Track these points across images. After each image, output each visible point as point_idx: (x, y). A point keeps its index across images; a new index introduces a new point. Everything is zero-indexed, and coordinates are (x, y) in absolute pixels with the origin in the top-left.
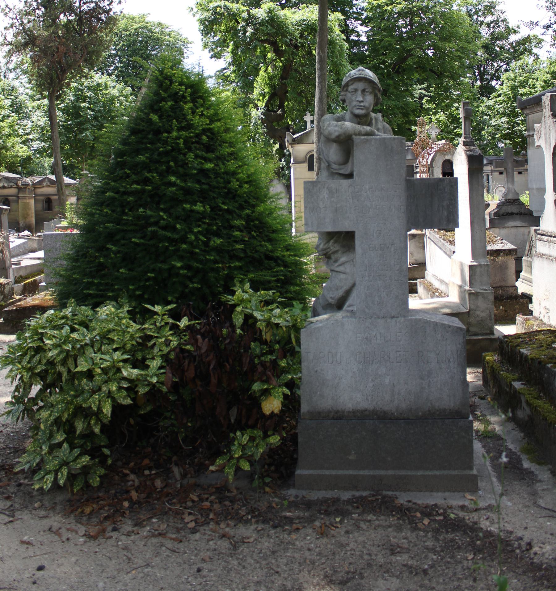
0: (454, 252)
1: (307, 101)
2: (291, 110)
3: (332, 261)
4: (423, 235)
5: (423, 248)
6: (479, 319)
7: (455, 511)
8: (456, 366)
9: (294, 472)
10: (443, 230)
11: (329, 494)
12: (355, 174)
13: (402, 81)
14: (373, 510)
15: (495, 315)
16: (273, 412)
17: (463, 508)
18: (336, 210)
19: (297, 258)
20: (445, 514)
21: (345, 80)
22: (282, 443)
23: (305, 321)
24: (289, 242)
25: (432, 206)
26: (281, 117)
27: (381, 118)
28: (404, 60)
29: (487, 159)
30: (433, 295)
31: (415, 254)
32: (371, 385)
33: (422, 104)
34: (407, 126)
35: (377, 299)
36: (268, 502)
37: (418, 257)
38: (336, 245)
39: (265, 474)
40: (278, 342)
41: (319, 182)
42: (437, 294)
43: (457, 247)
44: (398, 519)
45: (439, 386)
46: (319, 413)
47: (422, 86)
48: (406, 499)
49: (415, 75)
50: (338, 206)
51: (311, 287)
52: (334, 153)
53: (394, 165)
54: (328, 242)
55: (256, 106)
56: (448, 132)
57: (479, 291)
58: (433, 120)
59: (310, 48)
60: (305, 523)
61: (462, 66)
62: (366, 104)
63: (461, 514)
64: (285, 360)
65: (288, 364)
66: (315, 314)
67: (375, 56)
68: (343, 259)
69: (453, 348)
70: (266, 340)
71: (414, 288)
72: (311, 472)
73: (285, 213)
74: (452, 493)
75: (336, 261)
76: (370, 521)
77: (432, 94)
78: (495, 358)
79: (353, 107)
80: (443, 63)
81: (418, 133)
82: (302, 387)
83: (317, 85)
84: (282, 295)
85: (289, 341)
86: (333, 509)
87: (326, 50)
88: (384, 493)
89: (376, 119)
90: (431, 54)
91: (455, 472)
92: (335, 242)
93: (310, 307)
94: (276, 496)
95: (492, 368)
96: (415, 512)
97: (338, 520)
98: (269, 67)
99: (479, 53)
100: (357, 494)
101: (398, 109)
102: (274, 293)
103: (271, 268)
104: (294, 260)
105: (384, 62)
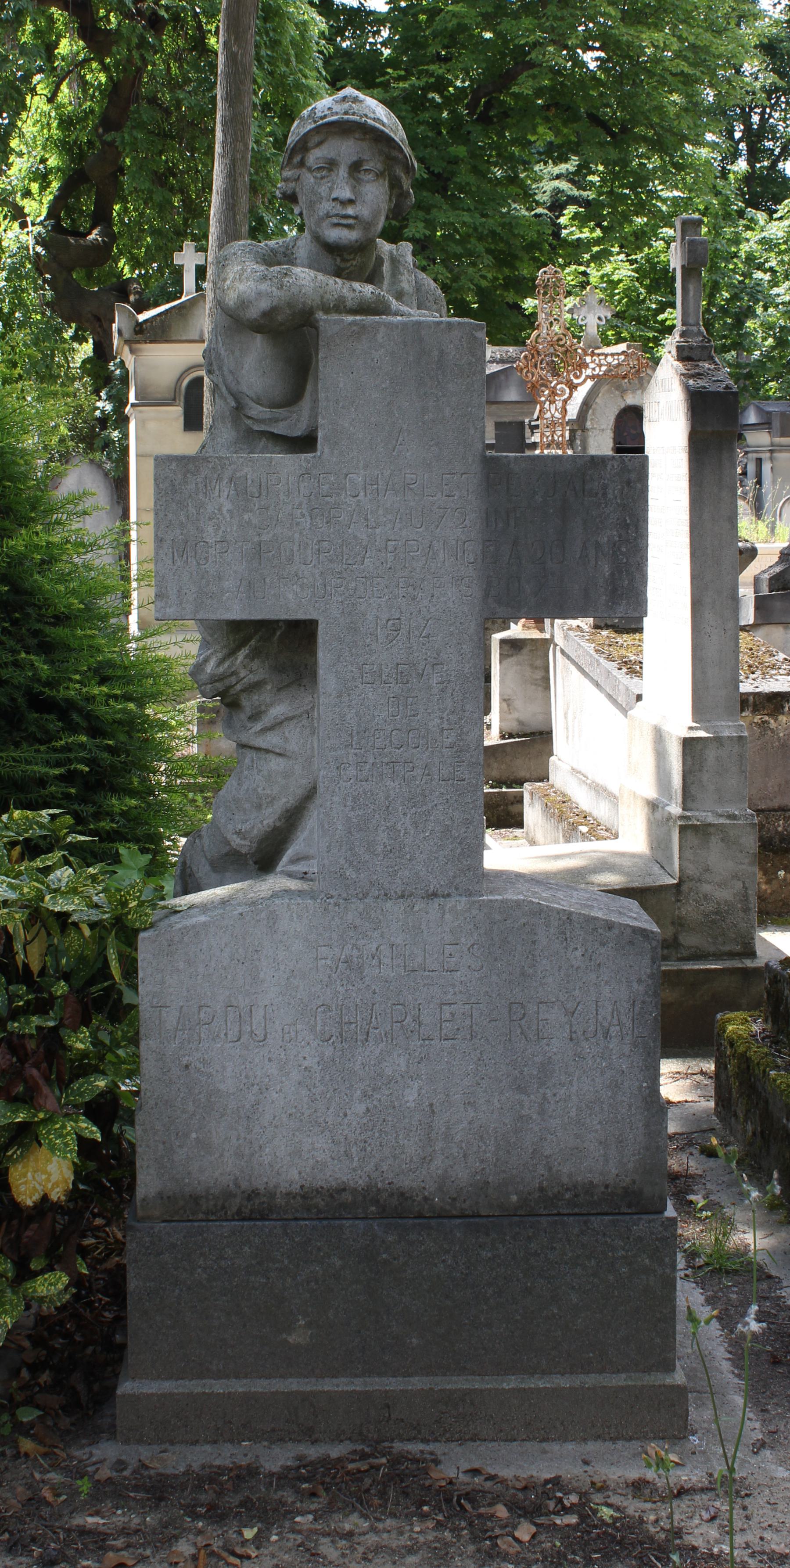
0: (639, 698)
1: (187, 203)
2: (135, 232)
3: (243, 716)
4: (546, 644)
5: (545, 683)
6: (710, 907)
7: (614, 1499)
8: (627, 1049)
9: (115, 1388)
10: (607, 627)
11: (226, 1455)
12: (320, 434)
13: (500, 149)
14: (360, 1502)
15: (761, 898)
16: (45, 1198)
17: (638, 1487)
18: (258, 551)
19: (132, 706)
20: (584, 1510)
21: (298, 130)
22: (76, 1297)
23: (154, 906)
24: (110, 653)
25: (562, 543)
26: (102, 254)
27: (410, 258)
28: (508, 78)
29: (759, 410)
30: (571, 833)
31: (518, 703)
32: (361, 1108)
33: (559, 227)
34: (510, 297)
35: (382, 837)
36: (29, 1487)
37: (527, 713)
38: (255, 664)
39: (18, 1398)
40: (66, 977)
41: (206, 460)
42: (584, 829)
43: (649, 683)
44: (439, 1525)
45: (573, 1113)
46: (195, 1199)
47: (563, 168)
48: (466, 1466)
49: (541, 129)
50: (264, 538)
51: (177, 800)
52: (256, 368)
53: (447, 411)
54: (232, 653)
55: (18, 214)
56: (637, 322)
57: (711, 819)
58: (593, 280)
59: (199, 27)
60: (143, 1546)
61: (693, 107)
62: (363, 210)
63: (633, 1507)
64: (85, 1032)
65: (96, 1042)
66: (188, 885)
67: (415, 62)
68: (278, 710)
69: (618, 992)
70: (26, 966)
71: (513, 809)
72: (168, 1386)
73: (103, 559)
74: (609, 1444)
75: (255, 716)
76: (350, 1535)
77: (591, 195)
78: (756, 1028)
79: (321, 219)
80: (631, 96)
81: (541, 316)
82: (139, 1117)
83: (218, 149)
84: (80, 823)
85: (104, 972)
86: (235, 1500)
87: (252, 37)
88: (398, 1446)
89: (395, 261)
90: (592, 65)
91: (619, 1380)
92: (255, 654)
93: (173, 865)
94: (54, 1467)
95: (744, 1059)
96: (491, 1505)
97: (249, 1533)
98: (64, 87)
99: (747, 68)
100: (313, 1452)
101: (481, 238)
102: (53, 817)
103: (48, 739)
104: (124, 711)
105: (440, 85)
